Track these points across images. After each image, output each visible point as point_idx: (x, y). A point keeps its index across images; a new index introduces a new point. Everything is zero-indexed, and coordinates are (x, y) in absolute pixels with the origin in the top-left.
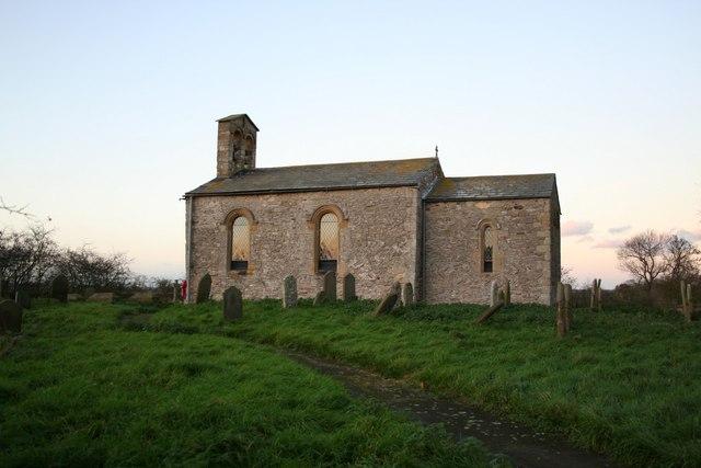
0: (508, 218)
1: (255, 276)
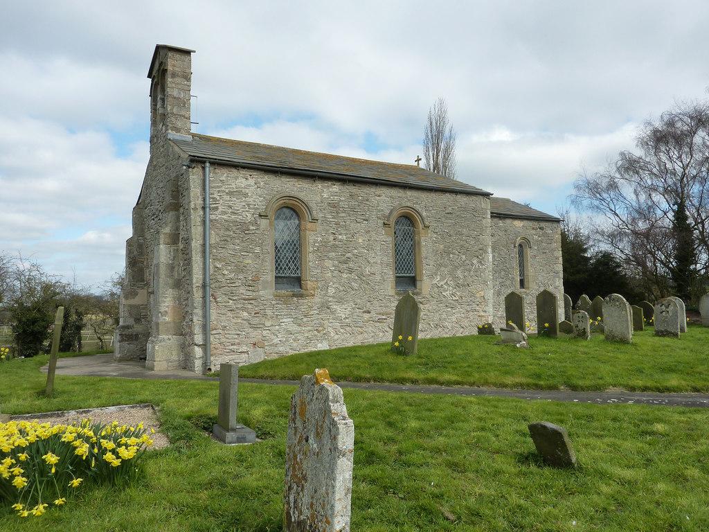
0: (536, 237)
1: (317, 299)
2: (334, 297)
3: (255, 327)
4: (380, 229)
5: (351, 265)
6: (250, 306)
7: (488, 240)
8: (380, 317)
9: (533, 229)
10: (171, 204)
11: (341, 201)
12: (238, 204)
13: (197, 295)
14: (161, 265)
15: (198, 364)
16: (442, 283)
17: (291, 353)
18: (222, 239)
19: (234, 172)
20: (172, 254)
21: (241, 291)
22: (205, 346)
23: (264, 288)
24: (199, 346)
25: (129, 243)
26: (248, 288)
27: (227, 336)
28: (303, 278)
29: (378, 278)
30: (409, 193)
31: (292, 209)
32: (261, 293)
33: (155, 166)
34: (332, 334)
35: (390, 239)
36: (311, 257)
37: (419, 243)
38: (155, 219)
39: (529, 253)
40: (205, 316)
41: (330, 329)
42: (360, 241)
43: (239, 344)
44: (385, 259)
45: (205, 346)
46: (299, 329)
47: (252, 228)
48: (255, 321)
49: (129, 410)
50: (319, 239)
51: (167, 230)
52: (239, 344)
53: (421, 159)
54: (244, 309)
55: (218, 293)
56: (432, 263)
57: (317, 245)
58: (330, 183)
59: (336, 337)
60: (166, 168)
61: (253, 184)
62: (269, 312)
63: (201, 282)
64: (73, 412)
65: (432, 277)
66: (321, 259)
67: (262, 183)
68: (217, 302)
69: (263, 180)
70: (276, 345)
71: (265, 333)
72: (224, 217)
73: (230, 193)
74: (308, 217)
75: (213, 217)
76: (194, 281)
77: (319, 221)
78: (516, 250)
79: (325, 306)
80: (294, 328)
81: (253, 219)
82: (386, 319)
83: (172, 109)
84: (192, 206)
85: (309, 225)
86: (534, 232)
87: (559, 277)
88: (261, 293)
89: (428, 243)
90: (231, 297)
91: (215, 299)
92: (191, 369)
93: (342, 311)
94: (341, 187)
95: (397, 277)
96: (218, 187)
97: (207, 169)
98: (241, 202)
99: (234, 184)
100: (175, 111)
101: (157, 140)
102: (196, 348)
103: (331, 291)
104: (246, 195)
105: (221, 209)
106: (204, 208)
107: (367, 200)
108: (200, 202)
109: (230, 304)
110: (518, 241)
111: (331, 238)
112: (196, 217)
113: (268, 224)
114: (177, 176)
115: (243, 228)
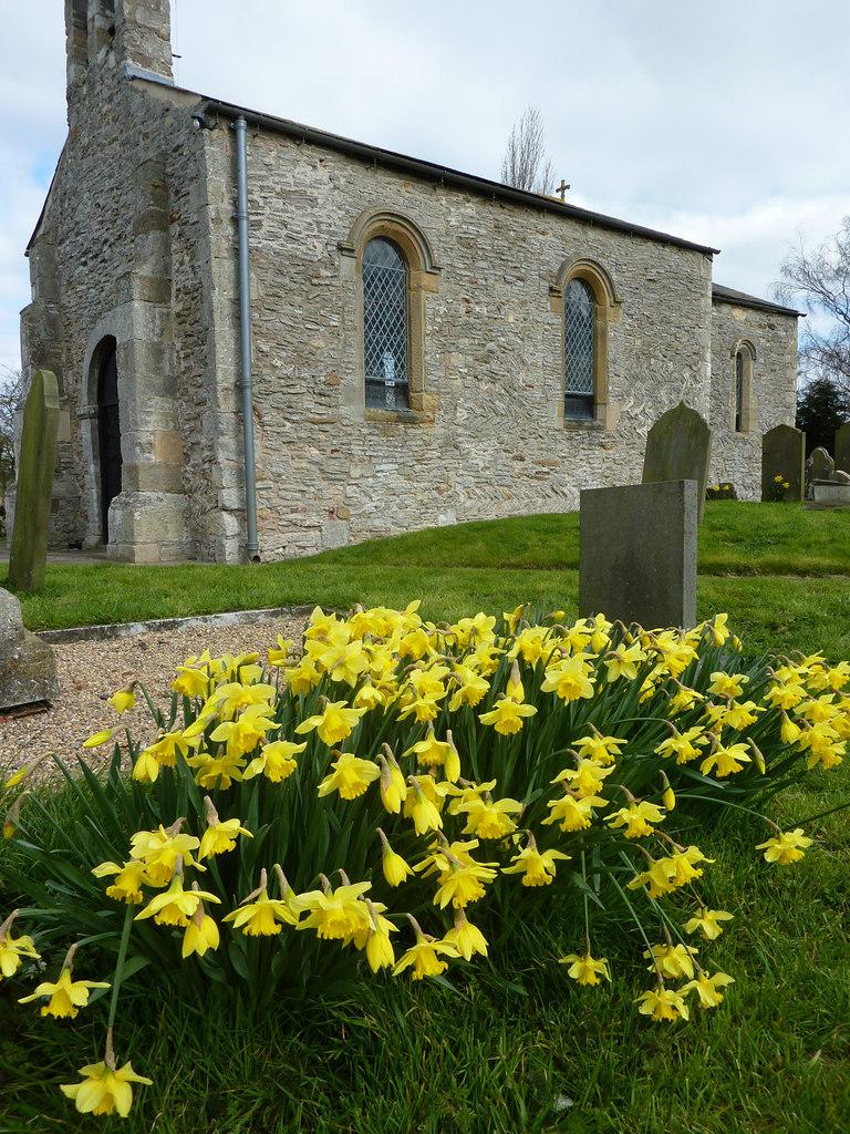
1: (438, 430)
2: (465, 426)
3: (332, 479)
4: (544, 300)
5: (495, 366)
6: (322, 436)
7: (706, 336)
8: (540, 468)
9: (760, 326)
10: (151, 214)
11: (479, 235)
12: (300, 220)
13: (227, 406)
14: (138, 345)
15: (231, 548)
16: (637, 411)
17: (396, 532)
18: (271, 291)
19: (292, 150)
20: (158, 322)
21: (307, 405)
22: (244, 513)
23: (349, 401)
24: (231, 511)
25: (27, 315)
26: (318, 399)
27: (282, 493)
28: (414, 385)
29: (538, 394)
30: (593, 235)
31: (396, 242)
32: (343, 410)
33: (85, 149)
34: (462, 498)
35: (559, 321)
36: (428, 344)
37: (604, 332)
38: (91, 264)
39: (753, 368)
40: (243, 450)
41: (459, 488)
42: (511, 319)
43: (304, 510)
44: (550, 359)
45: (244, 513)
46: (407, 485)
47: (324, 273)
48: (333, 466)
49: (268, 620)
50: (443, 309)
51: (146, 270)
52: (304, 510)
53: (568, 187)
54: (312, 441)
55: (265, 406)
56: (623, 372)
57: (439, 320)
58: (461, 196)
59: (468, 504)
60: (123, 144)
61: (325, 178)
62: (356, 450)
63: (232, 380)
64: (138, 628)
65: (621, 398)
66: (445, 350)
67: (343, 181)
68: (263, 425)
69: (346, 173)
70: (368, 515)
71: (350, 490)
72: (274, 244)
73: (284, 195)
74: (424, 264)
75: (254, 243)
76: (220, 376)
77: (443, 273)
78: (734, 362)
79: (451, 444)
80: (399, 483)
81: (326, 254)
82: (548, 473)
83: (132, 13)
84: (213, 214)
85: (426, 279)
86: (760, 332)
87: (790, 415)
88: (343, 410)
89: (618, 330)
90: (288, 416)
91: (259, 416)
92: (215, 556)
93: (480, 453)
94: (480, 208)
95: (567, 396)
96: (261, 178)
97: (242, 134)
98: (304, 215)
99: (289, 175)
100: (139, 16)
101: (92, 88)
102: (226, 517)
103: (462, 415)
104: (313, 201)
105: (266, 228)
106: (236, 221)
107: (524, 240)
108: (226, 206)
109: (286, 429)
110: (739, 346)
111: (462, 309)
112: (220, 237)
113: (354, 268)
114: (164, 155)
115: (308, 272)
